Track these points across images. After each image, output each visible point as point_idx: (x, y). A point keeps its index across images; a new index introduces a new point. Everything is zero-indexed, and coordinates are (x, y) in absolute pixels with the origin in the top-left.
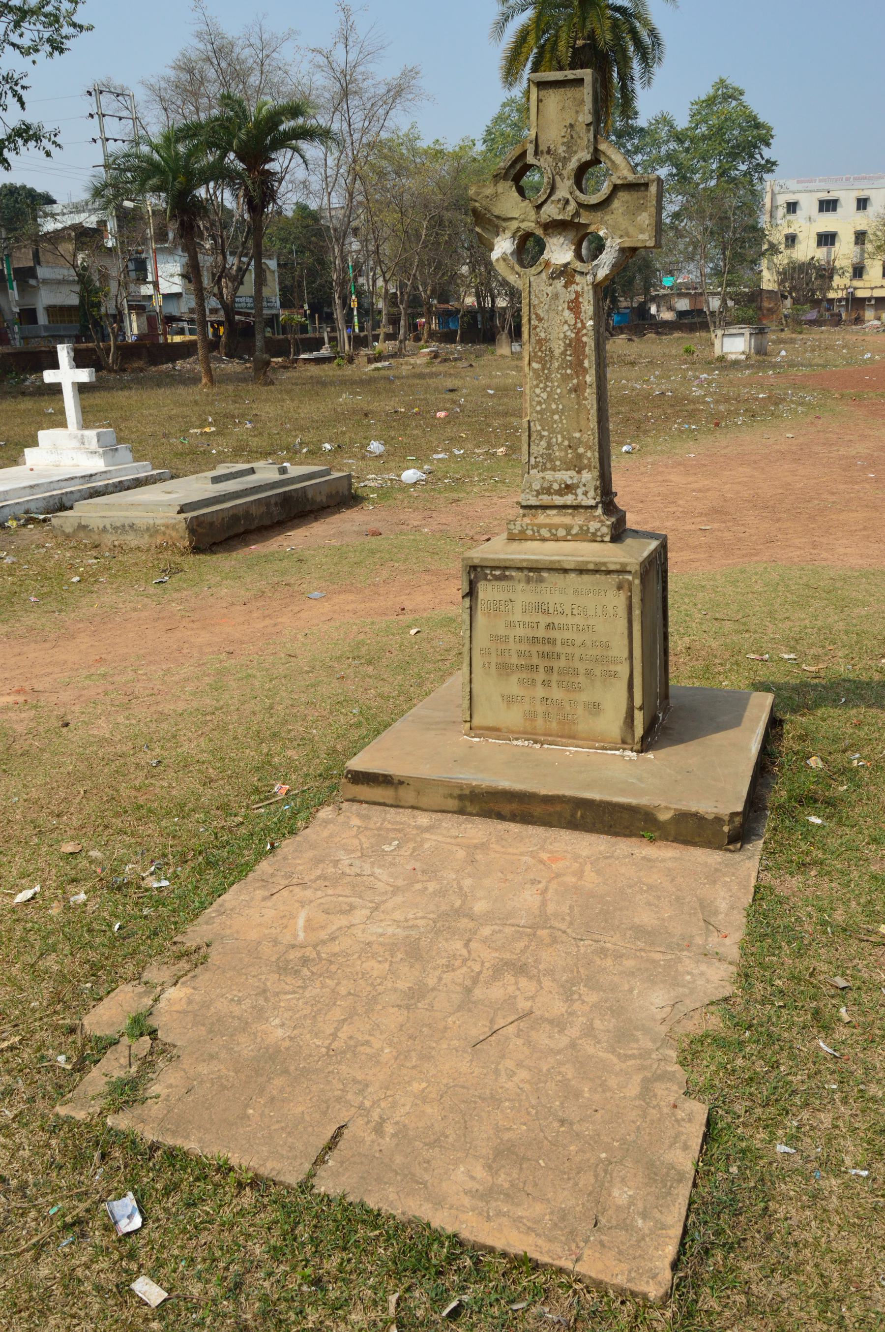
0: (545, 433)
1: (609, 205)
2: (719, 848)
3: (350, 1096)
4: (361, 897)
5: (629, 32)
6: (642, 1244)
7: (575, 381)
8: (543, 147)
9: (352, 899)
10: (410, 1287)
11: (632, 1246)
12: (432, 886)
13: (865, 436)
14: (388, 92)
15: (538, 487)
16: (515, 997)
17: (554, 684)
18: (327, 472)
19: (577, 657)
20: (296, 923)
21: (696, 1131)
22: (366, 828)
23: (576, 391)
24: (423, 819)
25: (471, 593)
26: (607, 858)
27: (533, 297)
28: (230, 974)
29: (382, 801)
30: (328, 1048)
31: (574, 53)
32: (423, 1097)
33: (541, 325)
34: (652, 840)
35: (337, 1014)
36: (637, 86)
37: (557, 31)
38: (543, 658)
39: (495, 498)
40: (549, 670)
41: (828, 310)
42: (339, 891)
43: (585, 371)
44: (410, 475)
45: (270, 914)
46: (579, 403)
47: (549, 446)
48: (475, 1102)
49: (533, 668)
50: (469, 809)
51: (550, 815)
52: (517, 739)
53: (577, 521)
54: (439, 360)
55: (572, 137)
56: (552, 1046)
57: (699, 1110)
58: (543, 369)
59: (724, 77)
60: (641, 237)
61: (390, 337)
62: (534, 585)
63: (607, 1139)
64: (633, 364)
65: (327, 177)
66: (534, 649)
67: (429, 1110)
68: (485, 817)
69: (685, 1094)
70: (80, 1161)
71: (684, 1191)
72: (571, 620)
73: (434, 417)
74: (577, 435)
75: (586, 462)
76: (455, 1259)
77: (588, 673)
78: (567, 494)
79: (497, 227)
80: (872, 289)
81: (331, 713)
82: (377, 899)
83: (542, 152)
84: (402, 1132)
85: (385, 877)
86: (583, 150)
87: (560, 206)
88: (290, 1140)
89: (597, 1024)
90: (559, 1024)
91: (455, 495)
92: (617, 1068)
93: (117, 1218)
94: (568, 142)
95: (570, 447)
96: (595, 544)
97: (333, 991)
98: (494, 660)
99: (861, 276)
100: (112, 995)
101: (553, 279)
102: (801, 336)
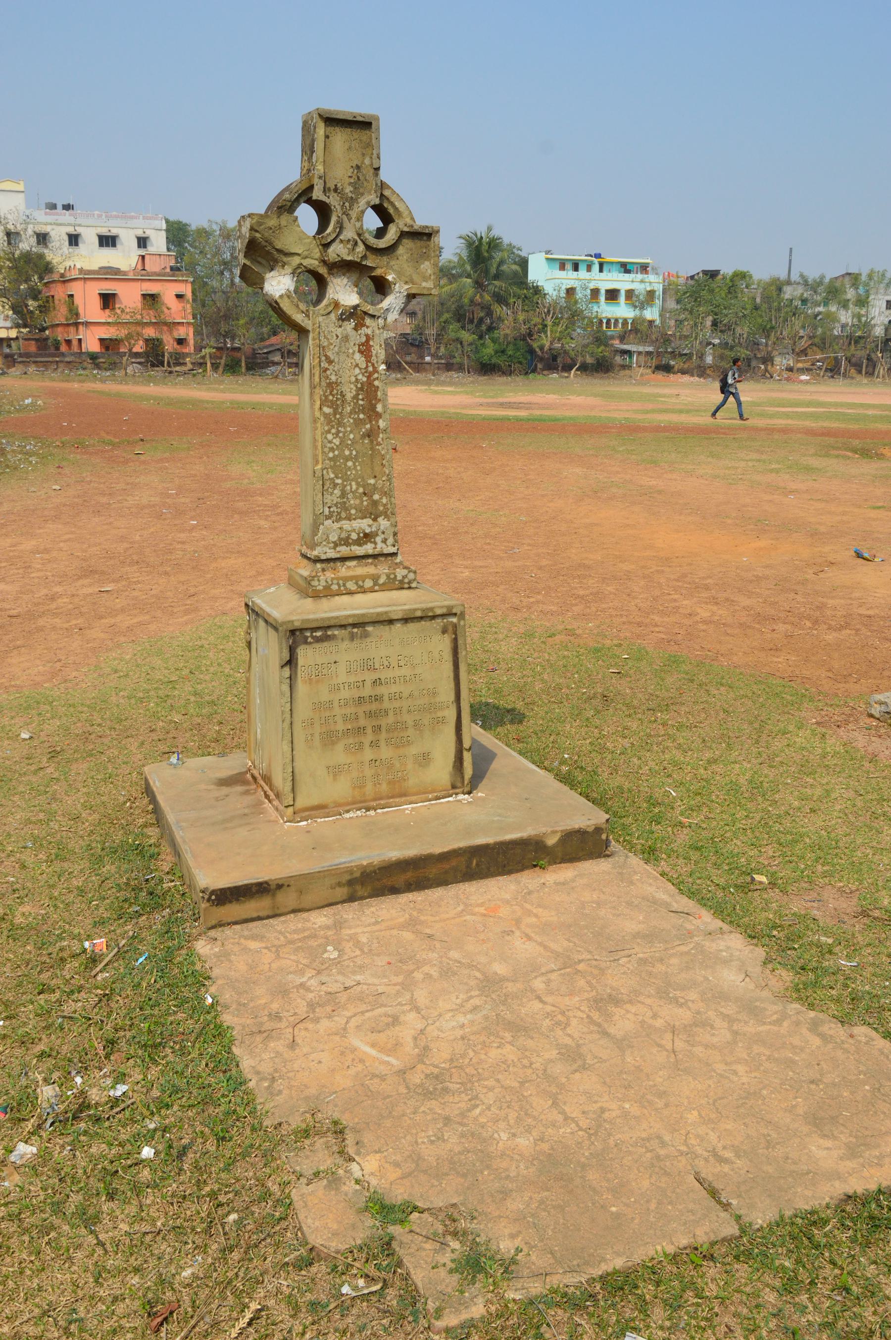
0: (339, 481)
1: (394, 251)
7: (368, 426)
17: (382, 743)
19: (404, 710)
23: (369, 436)
24: (319, 919)
25: (291, 662)
27: (322, 338)
29: (255, 915)
33: (331, 367)
38: (371, 718)
40: (377, 729)
46: (372, 449)
47: (343, 494)
49: (361, 730)
50: (360, 893)
51: (446, 872)
52: (348, 811)
55: (358, 178)
58: (335, 414)
60: (424, 284)
62: (359, 641)
66: (360, 710)
68: (377, 896)
72: (398, 672)
74: (372, 481)
75: (381, 508)
77: (416, 725)
78: (365, 543)
83: (329, 189)
87: (349, 246)
94: (355, 183)
95: (365, 494)
98: (317, 729)
101: (343, 320)
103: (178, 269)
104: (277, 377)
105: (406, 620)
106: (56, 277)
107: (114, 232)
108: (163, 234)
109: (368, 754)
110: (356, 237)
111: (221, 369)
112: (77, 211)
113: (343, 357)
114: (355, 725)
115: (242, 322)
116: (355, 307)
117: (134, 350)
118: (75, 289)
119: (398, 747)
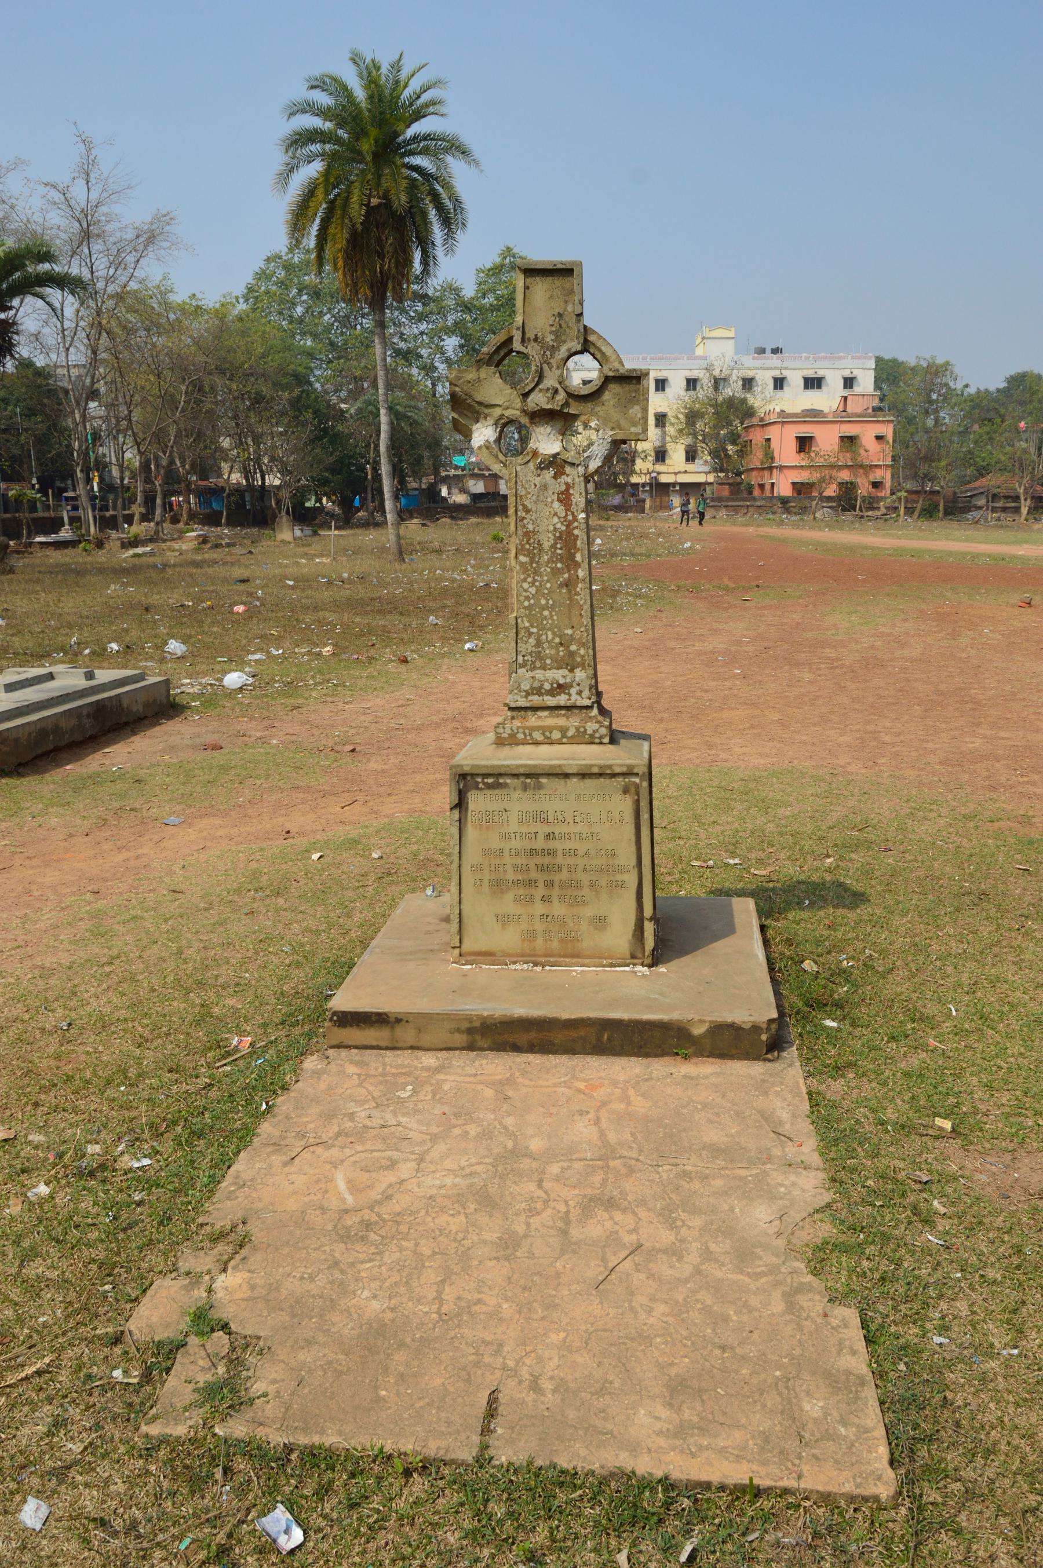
0: (534, 630)
2: (758, 1058)
3: (487, 1359)
4: (397, 1150)
5: (429, 194)
6: (854, 1450)
7: (566, 576)
8: (530, 335)
9: (389, 1153)
10: (634, 1541)
11: (845, 1454)
12: (473, 1130)
13: (716, 630)
14: (138, 237)
15: (528, 687)
16: (617, 1232)
17: (555, 900)
18: (141, 677)
19: (580, 868)
20: (336, 1186)
21: (855, 1335)
22: (368, 1076)
24: (429, 1059)
25: (461, 805)
26: (646, 1080)
27: (519, 488)
28: (286, 1250)
29: (375, 1043)
30: (438, 1312)
31: (367, 212)
32: (565, 1347)
34: (686, 1057)
35: (430, 1276)
36: (439, 252)
37: (349, 187)
38: (543, 872)
39: (341, 704)
41: (633, 495)
42: (369, 1146)
43: (577, 565)
44: (234, 679)
45: (300, 1180)
46: (570, 599)
48: (624, 1343)
49: (532, 883)
50: (480, 1044)
51: (573, 1040)
52: (515, 963)
53: (573, 722)
54: (209, 545)
56: (677, 1275)
57: (850, 1315)
58: (531, 563)
59: (511, 245)
60: (633, 430)
61: (145, 518)
63: (775, 1358)
64: (439, 552)
65: (63, 330)
66: (532, 863)
67: (580, 1360)
69: (830, 1301)
70: (198, 1483)
71: (870, 1395)
72: (573, 829)
73: (231, 612)
74: (569, 632)
75: (579, 660)
76: (672, 1503)
77: (593, 885)
78: (559, 694)
79: (478, 413)
80: (676, 474)
81: (257, 953)
82: (418, 1149)
84: (561, 1386)
85: (415, 1126)
86: (572, 340)
87: (549, 395)
88: (443, 1415)
89: (712, 1246)
90: (675, 1252)
91: (291, 701)
92: (753, 1287)
93: (274, 1536)
94: (557, 331)
96: (594, 747)
97: (415, 1252)
98: (487, 876)
99: (663, 460)
100: (149, 1293)
101: (542, 469)
102: (609, 523)
103: (880, 409)
104: (977, 522)
105: (583, 775)
106: (755, 421)
107: (820, 373)
108: (872, 373)
109: (539, 908)
110: (558, 386)
111: (916, 514)
112: (785, 355)
113: (540, 506)
114: (526, 877)
115: (943, 463)
116: (555, 456)
117: (826, 494)
118: (773, 433)
119: (571, 906)
